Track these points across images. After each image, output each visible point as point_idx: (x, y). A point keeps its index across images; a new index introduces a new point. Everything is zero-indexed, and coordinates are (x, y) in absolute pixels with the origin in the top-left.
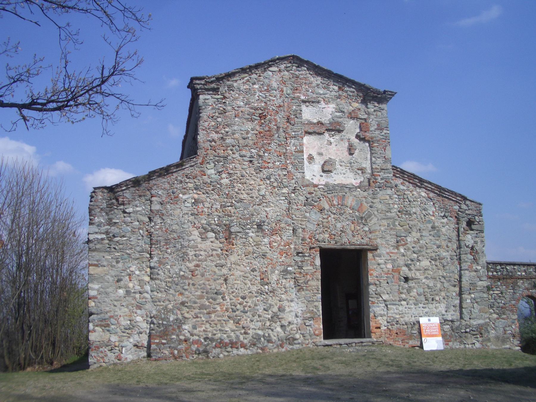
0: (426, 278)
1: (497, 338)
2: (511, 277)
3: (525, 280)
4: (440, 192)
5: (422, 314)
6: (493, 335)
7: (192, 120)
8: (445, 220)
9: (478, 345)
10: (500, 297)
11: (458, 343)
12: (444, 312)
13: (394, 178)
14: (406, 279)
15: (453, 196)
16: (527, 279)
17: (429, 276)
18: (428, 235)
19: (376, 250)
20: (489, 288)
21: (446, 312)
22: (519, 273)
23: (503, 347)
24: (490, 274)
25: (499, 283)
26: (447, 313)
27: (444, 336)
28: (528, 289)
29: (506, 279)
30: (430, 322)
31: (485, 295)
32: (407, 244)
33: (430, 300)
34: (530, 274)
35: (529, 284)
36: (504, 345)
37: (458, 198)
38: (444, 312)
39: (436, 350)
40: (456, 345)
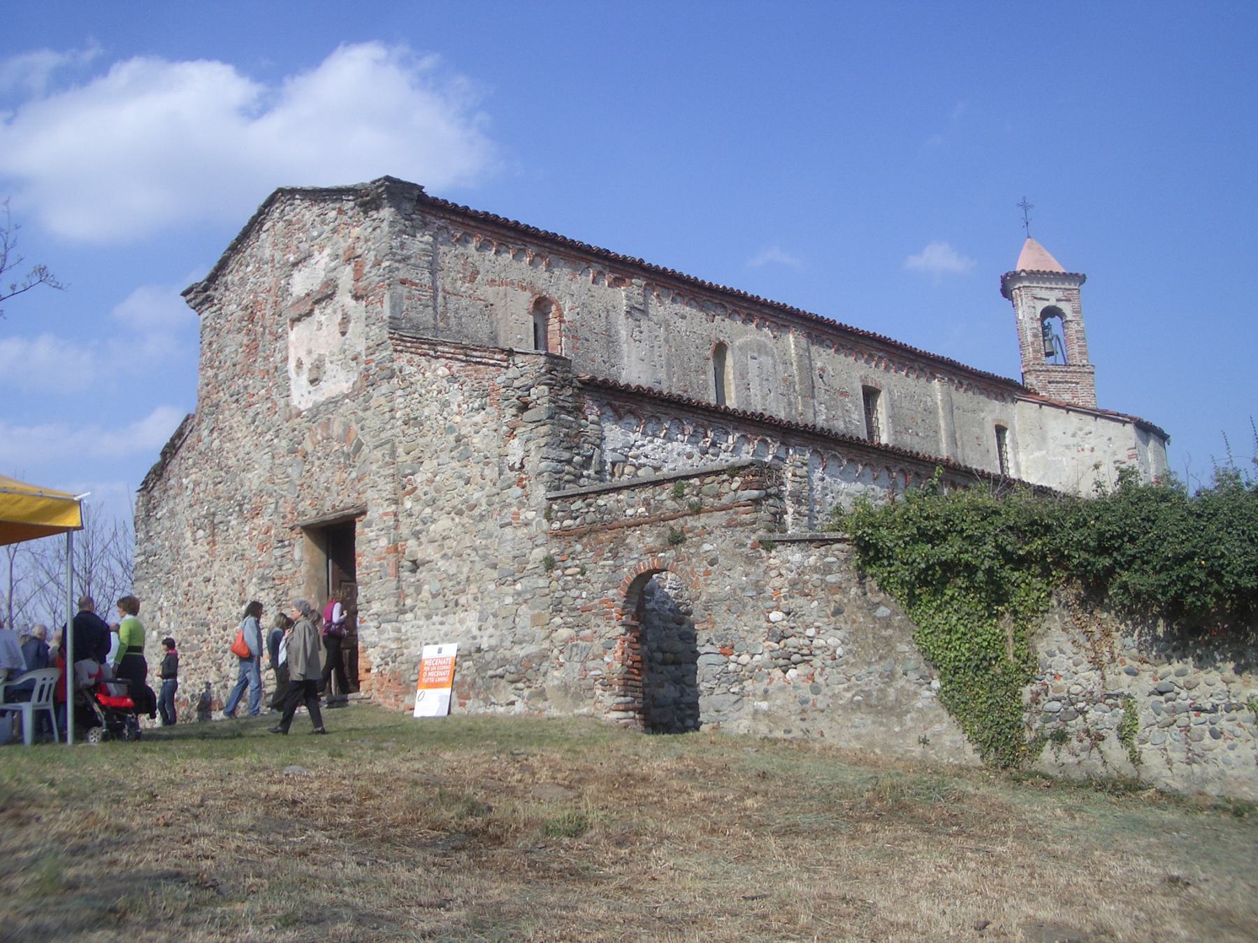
0: (444, 556)
1: (565, 688)
2: (607, 527)
3: (647, 526)
4: (466, 355)
5: (437, 639)
6: (556, 682)
7: (541, 332)
8: (478, 418)
9: (519, 707)
10: (578, 582)
11: (482, 703)
12: (475, 631)
13: (395, 355)
14: (415, 566)
15: (487, 354)
16: (651, 523)
17: (450, 552)
18: (448, 460)
19: (364, 513)
20: (550, 564)
21: (480, 629)
22: (630, 512)
23: (576, 711)
24: (556, 525)
25: (579, 547)
26: (482, 633)
27: (454, 686)
28: (652, 552)
29: (596, 531)
30: (441, 655)
31: (542, 582)
32: (416, 488)
33: (451, 604)
34: (657, 508)
35: (659, 535)
36: (577, 706)
37: (497, 357)
38: (475, 631)
39: (434, 718)
40: (475, 707)
